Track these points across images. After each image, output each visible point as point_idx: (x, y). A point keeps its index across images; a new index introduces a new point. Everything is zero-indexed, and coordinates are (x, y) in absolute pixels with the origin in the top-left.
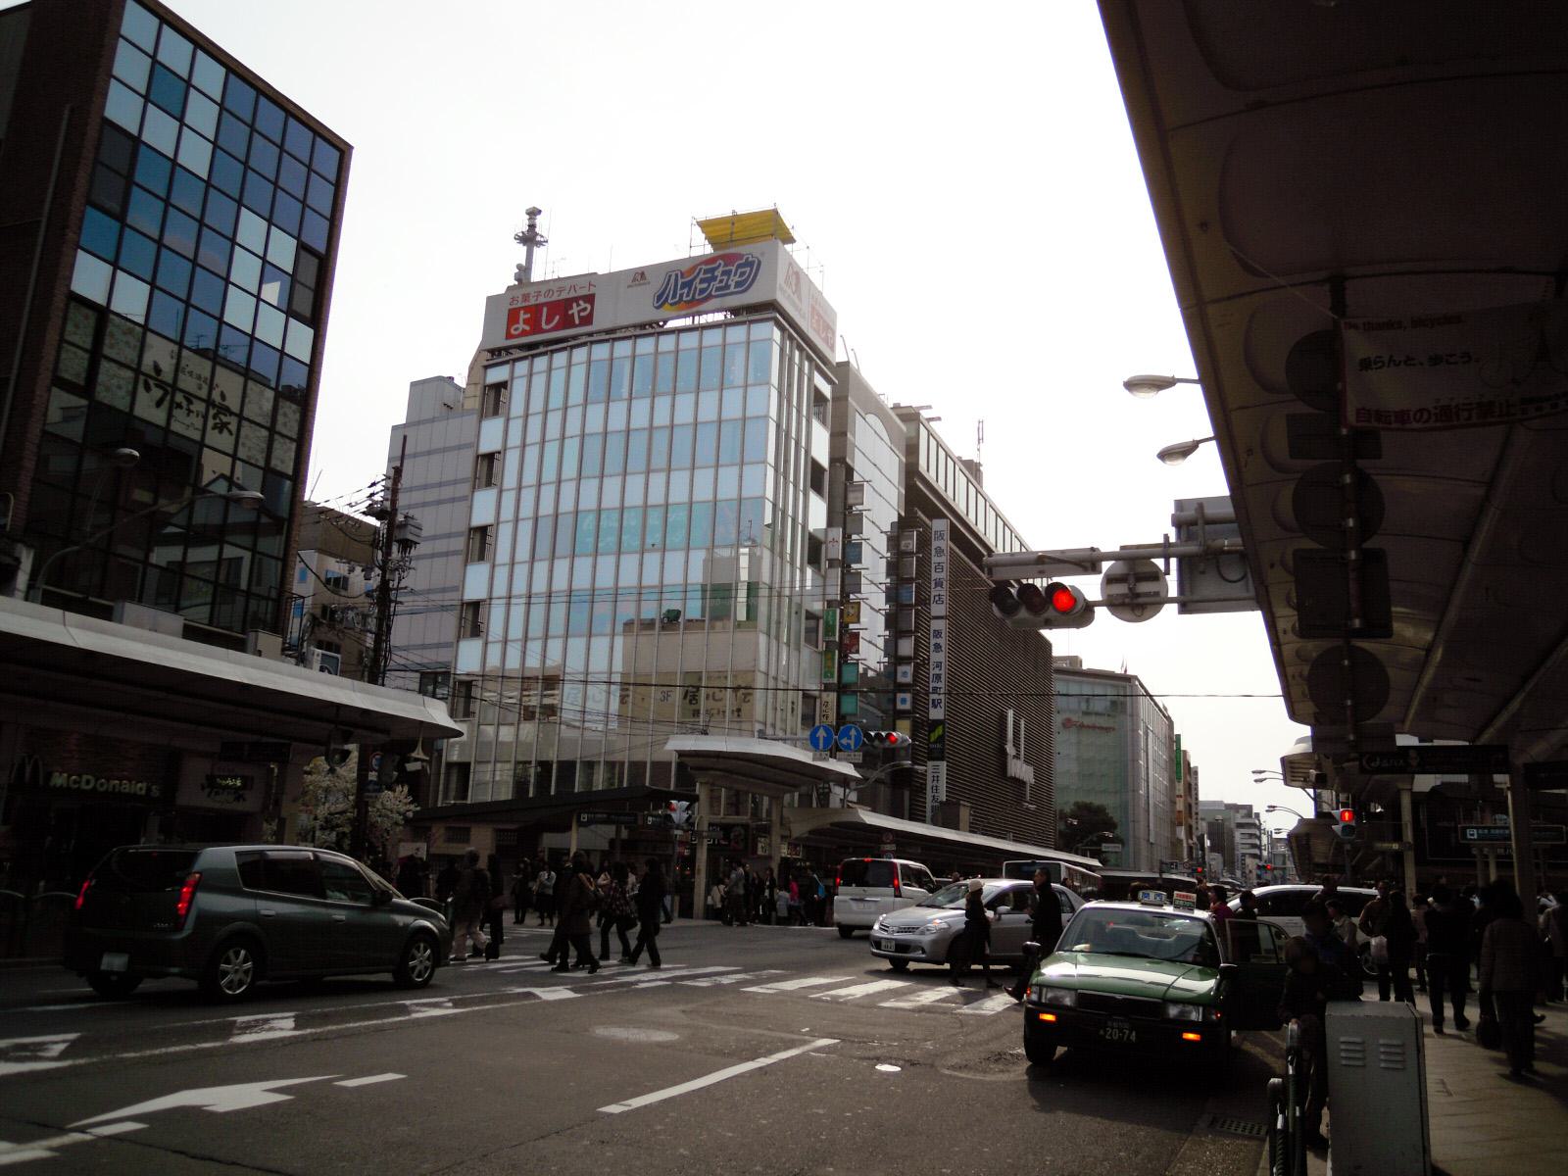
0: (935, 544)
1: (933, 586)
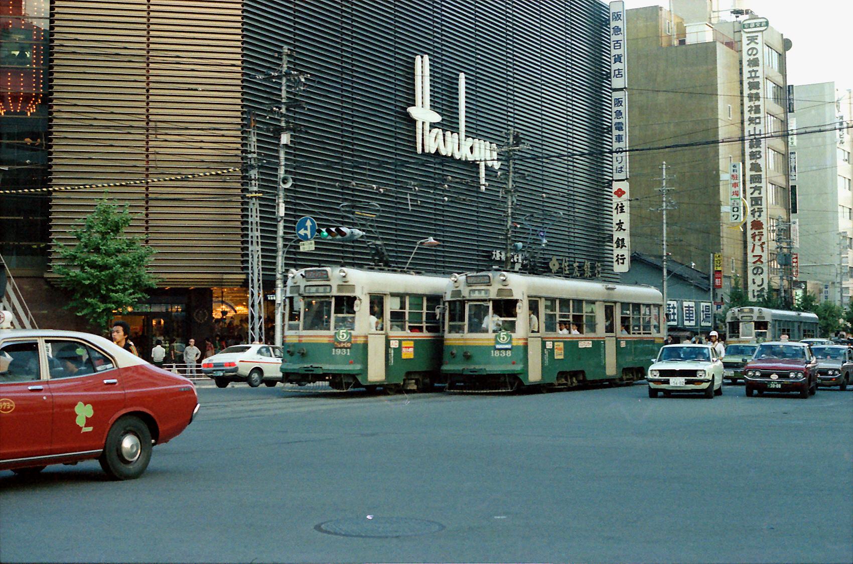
0: (613, 24)
1: (613, 61)
